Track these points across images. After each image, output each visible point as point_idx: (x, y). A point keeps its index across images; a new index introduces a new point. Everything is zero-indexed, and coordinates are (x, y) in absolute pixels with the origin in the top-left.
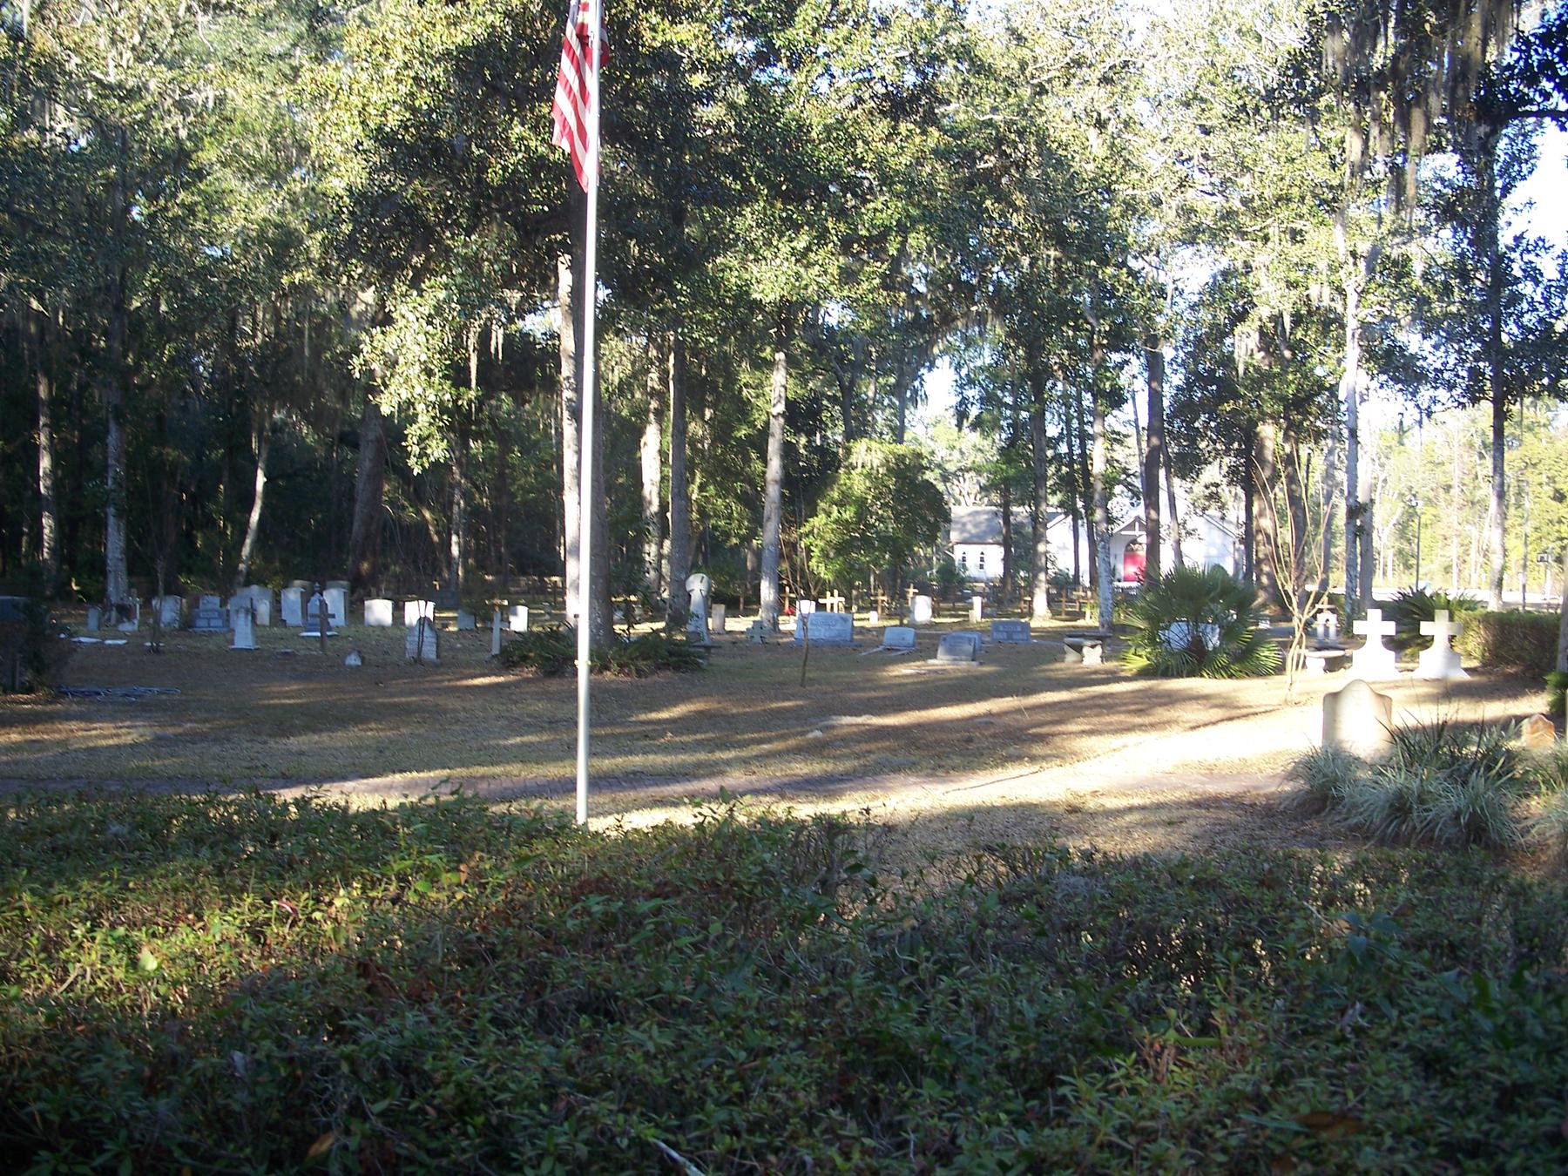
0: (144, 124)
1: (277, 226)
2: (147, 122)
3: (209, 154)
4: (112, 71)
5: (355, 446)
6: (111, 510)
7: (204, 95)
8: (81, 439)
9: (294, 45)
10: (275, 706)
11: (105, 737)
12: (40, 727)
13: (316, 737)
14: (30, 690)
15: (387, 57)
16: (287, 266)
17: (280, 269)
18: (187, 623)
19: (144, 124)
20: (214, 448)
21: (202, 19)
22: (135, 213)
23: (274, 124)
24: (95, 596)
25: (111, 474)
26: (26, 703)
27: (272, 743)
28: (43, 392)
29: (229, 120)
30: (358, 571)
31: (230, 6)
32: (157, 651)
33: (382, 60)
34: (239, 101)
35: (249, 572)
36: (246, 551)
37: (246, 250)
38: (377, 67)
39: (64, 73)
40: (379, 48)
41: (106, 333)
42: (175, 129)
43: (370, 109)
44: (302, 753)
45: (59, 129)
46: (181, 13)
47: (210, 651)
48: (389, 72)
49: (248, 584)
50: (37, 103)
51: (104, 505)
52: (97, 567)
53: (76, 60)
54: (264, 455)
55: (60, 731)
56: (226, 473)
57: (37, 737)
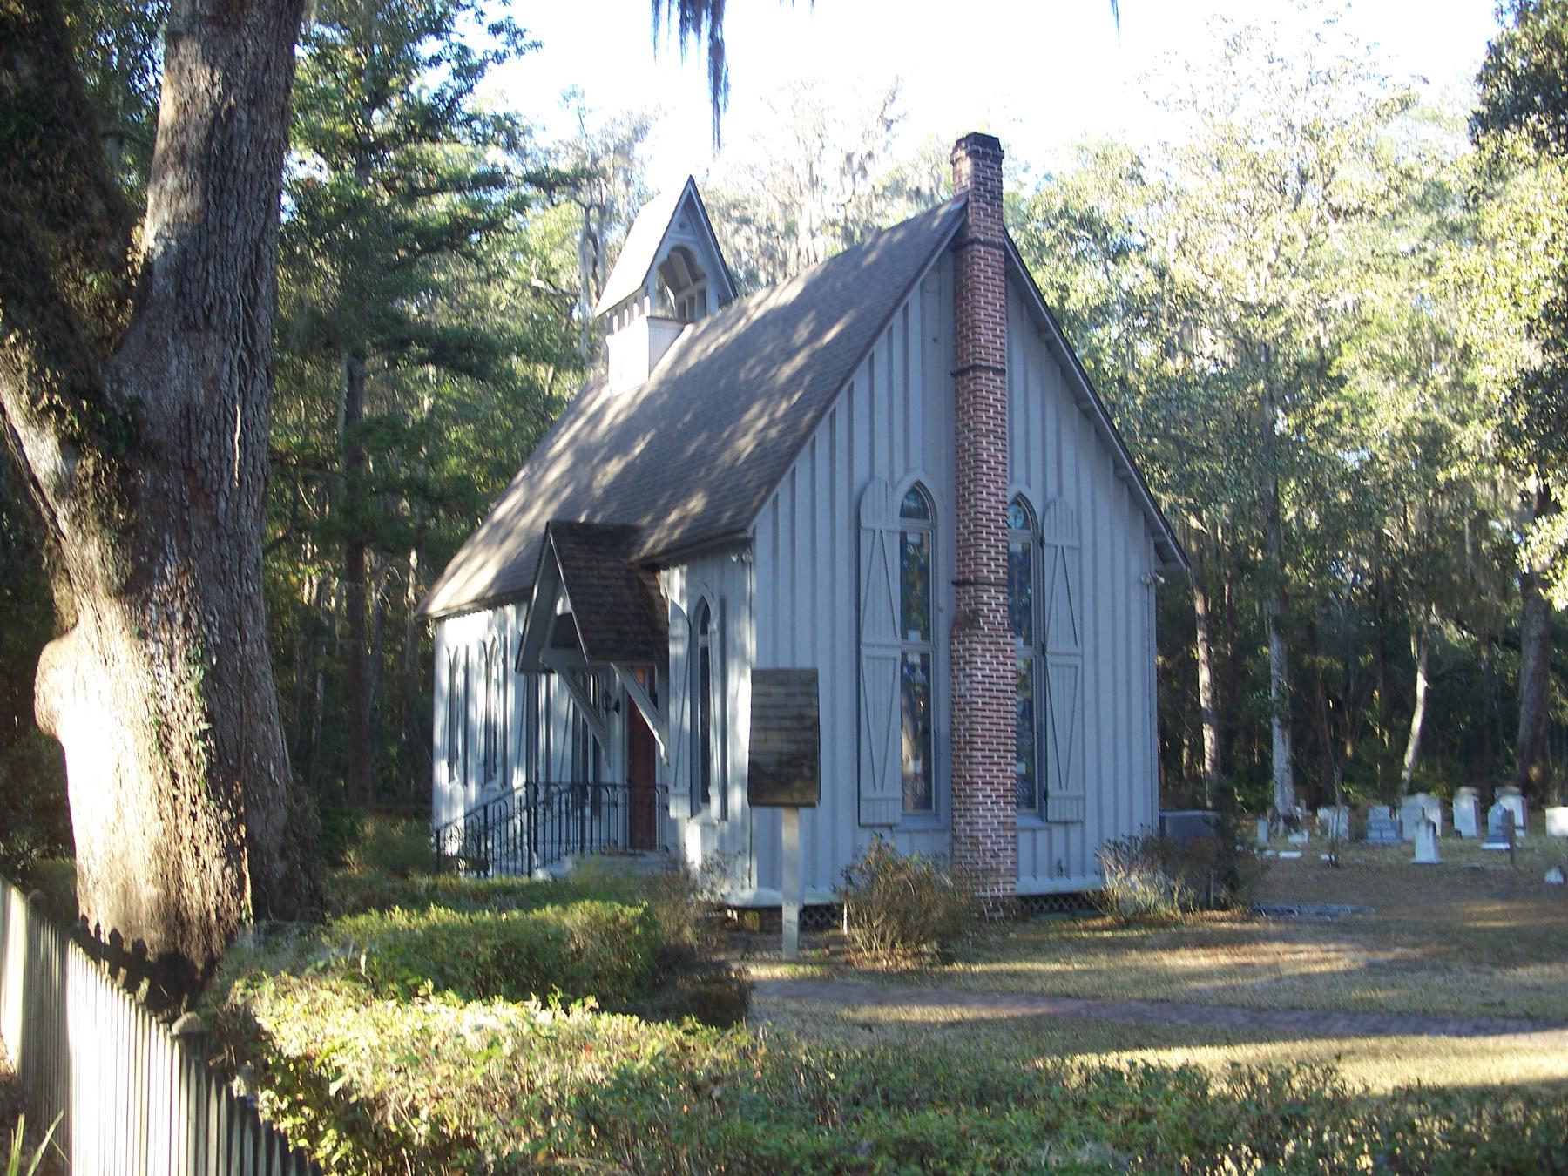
0: (1287, 336)
1: (1423, 424)
2: (1289, 335)
3: (1348, 359)
4: (1251, 290)
5: (1517, 648)
6: (1276, 721)
7: (1342, 302)
8: (1234, 653)
9: (1426, 239)
10: (1484, 930)
11: (1316, 962)
12: (1245, 948)
13: (1547, 969)
14: (1224, 908)
15: (1533, 233)
16: (1439, 463)
17: (1432, 466)
18: (1358, 835)
19: (1287, 336)
20: (1365, 653)
21: (1333, 226)
22: (1280, 427)
23: (1411, 320)
24: (1261, 806)
25: (1274, 684)
26: (1223, 921)
27: (1498, 974)
28: (1199, 608)
29: (1367, 323)
30: (1527, 775)
31: (1361, 210)
32: (1336, 865)
33: (1526, 237)
34: (1378, 300)
35: (1412, 781)
36: (1409, 758)
37: (1393, 449)
38: (1522, 245)
39: (1207, 299)
40: (1523, 224)
41: (1263, 546)
42: (1317, 339)
43: (1521, 289)
44: (1538, 988)
45: (1207, 354)
46: (1313, 224)
47: (1390, 865)
48: (1536, 247)
49: (1412, 791)
50: (1186, 331)
51: (1268, 717)
52: (1262, 774)
53: (1218, 285)
54: (1424, 658)
55: (1265, 954)
56: (1380, 679)
57: (1245, 960)
